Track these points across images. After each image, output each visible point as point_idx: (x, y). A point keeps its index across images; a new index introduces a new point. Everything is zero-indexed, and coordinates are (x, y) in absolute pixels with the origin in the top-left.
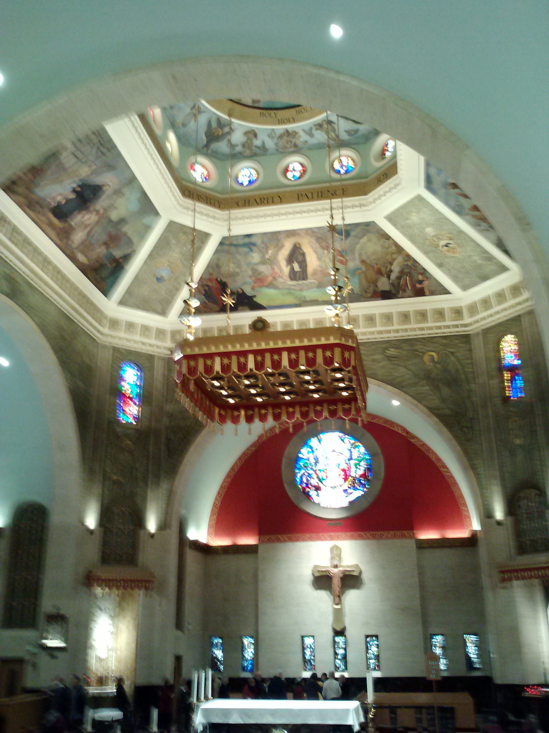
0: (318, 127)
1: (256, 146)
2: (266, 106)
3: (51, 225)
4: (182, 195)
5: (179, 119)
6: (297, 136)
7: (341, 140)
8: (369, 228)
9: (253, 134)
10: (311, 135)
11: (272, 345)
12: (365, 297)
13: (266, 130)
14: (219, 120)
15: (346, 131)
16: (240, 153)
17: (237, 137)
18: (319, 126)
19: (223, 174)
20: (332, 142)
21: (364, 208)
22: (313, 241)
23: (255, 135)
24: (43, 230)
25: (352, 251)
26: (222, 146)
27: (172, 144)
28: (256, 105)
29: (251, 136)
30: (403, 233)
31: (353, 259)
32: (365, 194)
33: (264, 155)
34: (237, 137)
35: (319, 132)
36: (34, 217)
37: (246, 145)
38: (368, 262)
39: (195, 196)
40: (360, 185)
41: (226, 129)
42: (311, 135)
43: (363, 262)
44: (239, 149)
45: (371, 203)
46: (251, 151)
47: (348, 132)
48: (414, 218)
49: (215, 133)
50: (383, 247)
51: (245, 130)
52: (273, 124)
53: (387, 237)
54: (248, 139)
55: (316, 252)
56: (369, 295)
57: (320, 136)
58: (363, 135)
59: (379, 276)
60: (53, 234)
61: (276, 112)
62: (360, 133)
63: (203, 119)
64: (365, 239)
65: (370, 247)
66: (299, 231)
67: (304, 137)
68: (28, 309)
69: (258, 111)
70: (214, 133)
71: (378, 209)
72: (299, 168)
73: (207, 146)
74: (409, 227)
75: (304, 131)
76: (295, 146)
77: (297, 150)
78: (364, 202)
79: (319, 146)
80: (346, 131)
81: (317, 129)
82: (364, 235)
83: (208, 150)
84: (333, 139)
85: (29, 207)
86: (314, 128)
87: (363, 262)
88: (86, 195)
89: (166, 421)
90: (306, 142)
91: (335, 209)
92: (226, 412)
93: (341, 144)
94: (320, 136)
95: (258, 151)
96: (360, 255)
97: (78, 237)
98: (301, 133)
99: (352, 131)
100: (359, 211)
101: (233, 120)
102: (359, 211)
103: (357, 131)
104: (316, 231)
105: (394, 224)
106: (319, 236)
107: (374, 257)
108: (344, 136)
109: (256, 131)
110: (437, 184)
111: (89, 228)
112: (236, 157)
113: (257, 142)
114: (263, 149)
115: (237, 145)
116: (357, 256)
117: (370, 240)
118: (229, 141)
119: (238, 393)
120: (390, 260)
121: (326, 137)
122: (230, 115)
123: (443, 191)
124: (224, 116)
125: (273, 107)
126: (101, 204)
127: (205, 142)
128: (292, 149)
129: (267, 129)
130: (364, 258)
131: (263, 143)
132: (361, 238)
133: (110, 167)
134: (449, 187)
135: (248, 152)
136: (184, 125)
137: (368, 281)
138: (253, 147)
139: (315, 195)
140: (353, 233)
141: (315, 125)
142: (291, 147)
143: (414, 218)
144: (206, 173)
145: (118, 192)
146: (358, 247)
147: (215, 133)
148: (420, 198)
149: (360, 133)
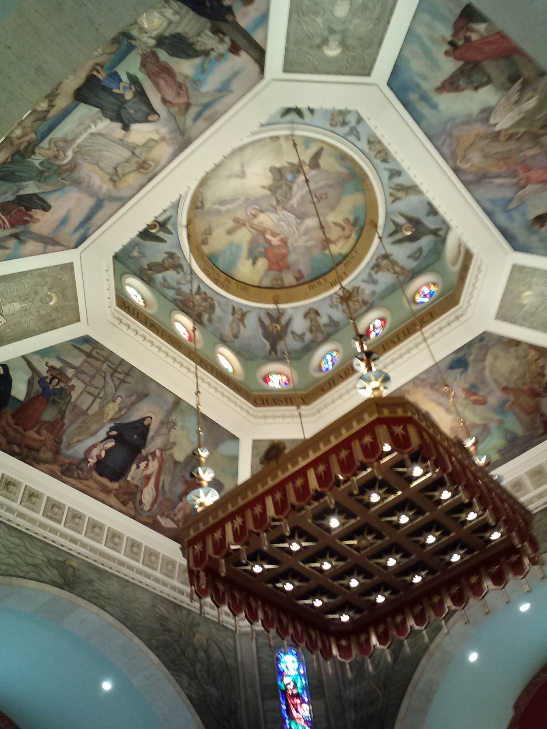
0: (376, 269)
1: (325, 325)
2: (313, 277)
3: (107, 490)
4: (255, 406)
5: (227, 332)
6: (360, 291)
7: (410, 271)
8: (484, 342)
9: (312, 314)
10: (375, 282)
11: (291, 470)
12: (539, 436)
13: (323, 299)
14: (269, 314)
15: (409, 257)
16: (312, 341)
17: (300, 325)
18: (377, 267)
19: (303, 371)
20: (402, 278)
21: (462, 319)
22: (428, 391)
23: (317, 313)
24: (103, 502)
25: (483, 381)
26: (290, 343)
27: (227, 360)
28: (302, 281)
29: (313, 316)
30: (531, 327)
31: (491, 392)
32: (456, 303)
33: (337, 331)
34: (300, 325)
35: (380, 274)
36: (80, 486)
37: (314, 329)
38: (511, 386)
39: (270, 401)
40: (448, 300)
41: (284, 321)
42: (375, 282)
43: (505, 389)
44: (308, 337)
45: (467, 308)
46: (321, 333)
47: (411, 256)
48: (528, 297)
49: (275, 333)
50: (518, 358)
51: (302, 312)
52: (326, 290)
53: (517, 343)
54: (311, 321)
55: (440, 404)
56: (541, 431)
57: (385, 278)
58: (430, 251)
59: (538, 399)
60: (113, 500)
61: (324, 277)
62: (425, 252)
63: (251, 321)
64: (489, 360)
65: (502, 367)
66: (406, 387)
67: (368, 289)
68: (98, 600)
69: (306, 287)
70: (272, 332)
71: (481, 311)
72: (378, 323)
73: (273, 349)
74: (533, 314)
75: (364, 281)
76: (365, 303)
77: (369, 306)
78: (460, 313)
79: (391, 290)
80: (409, 257)
81: (376, 272)
82: (485, 355)
83: (276, 354)
84: (402, 274)
85: (63, 473)
86: (373, 273)
87: (505, 389)
88: (131, 440)
89: (351, 715)
90: (373, 293)
91: (429, 338)
92: (348, 640)
93: (414, 274)
94: (385, 278)
95: (329, 330)
96: (496, 381)
97: (148, 495)
98: (363, 286)
99: (416, 253)
100: (458, 326)
101: (281, 306)
102: (458, 326)
103: (420, 250)
104: (424, 376)
105: (513, 321)
106: (432, 381)
107: (515, 377)
108: (411, 264)
109: (316, 307)
110: (522, 237)
111: (153, 480)
112: (309, 348)
113: (323, 320)
114: (334, 325)
115: (304, 334)
116: (493, 386)
117: (496, 358)
118: (293, 333)
119: (313, 584)
120: (539, 370)
121: (394, 276)
122: (276, 302)
123: (534, 240)
124: (271, 306)
125: (319, 274)
126: (154, 444)
127: (269, 346)
128: (364, 308)
129: (324, 299)
130: (504, 384)
131: (330, 317)
132: (484, 360)
133: (143, 396)
134: (536, 227)
135: (320, 336)
136: (236, 336)
137: (528, 413)
138: (322, 328)
139: (401, 336)
140: (471, 359)
141: (372, 269)
142: (361, 307)
143: (528, 297)
144: (284, 379)
145: (168, 424)
146: (487, 373)
147: (275, 333)
148: (517, 269)
149: (425, 252)
